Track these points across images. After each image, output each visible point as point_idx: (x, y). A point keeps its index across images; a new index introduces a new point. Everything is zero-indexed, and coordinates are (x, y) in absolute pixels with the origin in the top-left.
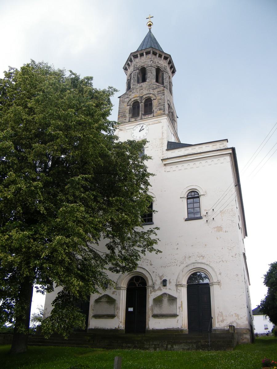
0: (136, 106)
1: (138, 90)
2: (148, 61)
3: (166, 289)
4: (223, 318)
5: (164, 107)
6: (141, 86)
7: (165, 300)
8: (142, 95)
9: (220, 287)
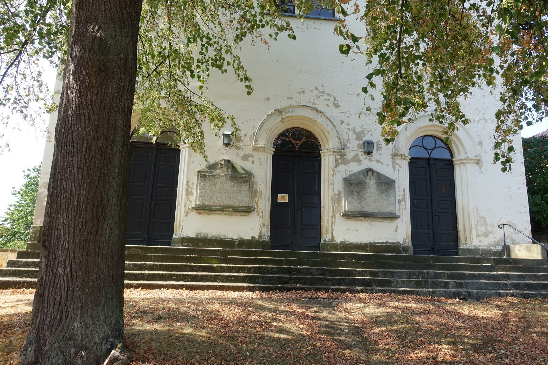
7: (371, 183)
9: (480, 169)
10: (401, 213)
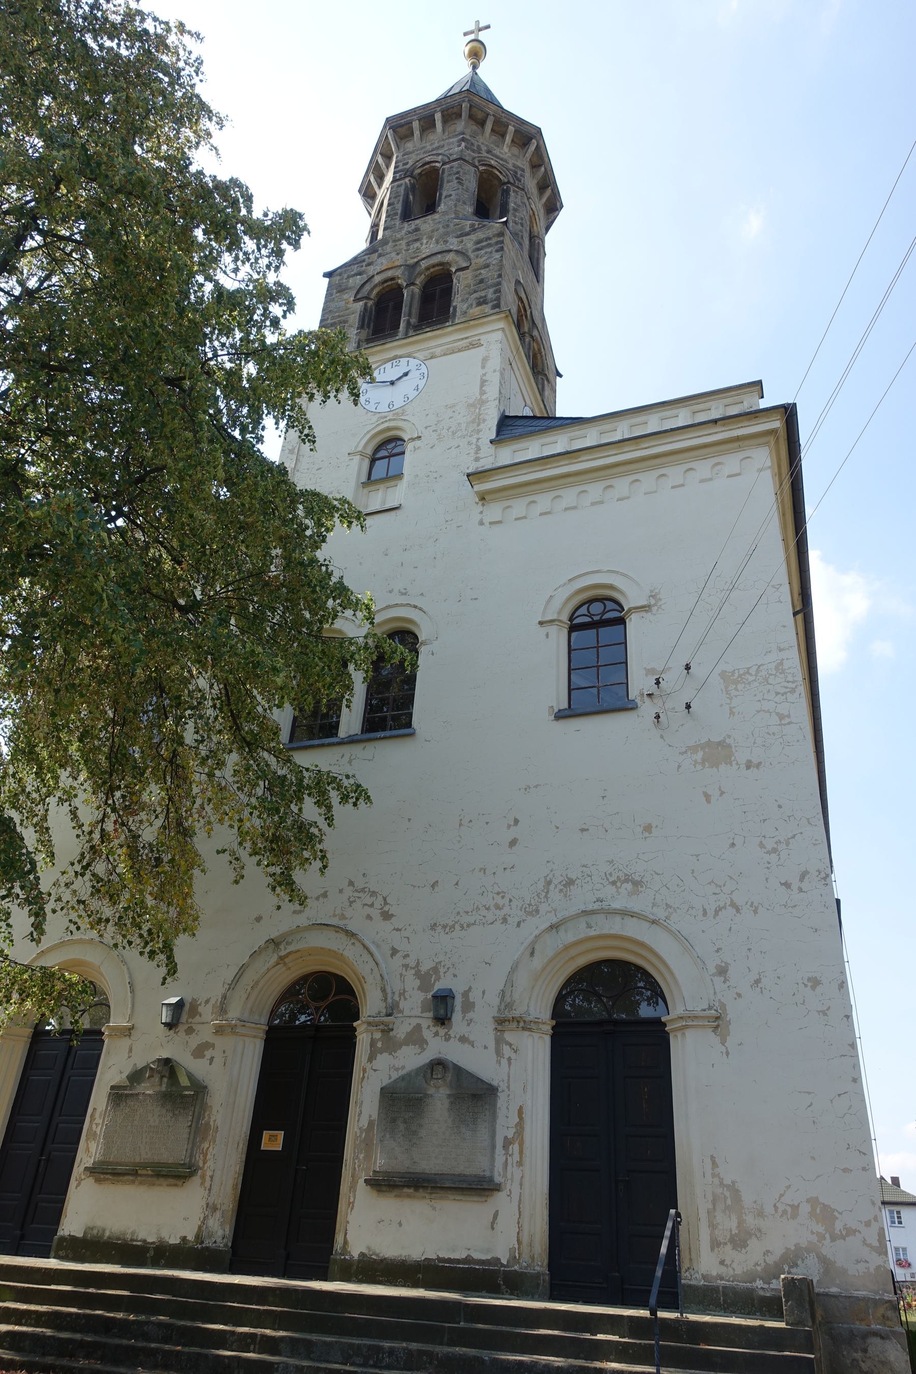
0: (391, 304)
1: (403, 243)
2: (449, 144)
3: (447, 1038)
4: (740, 1223)
5: (498, 291)
6: (417, 230)
8: (416, 260)
10: (509, 1176)
